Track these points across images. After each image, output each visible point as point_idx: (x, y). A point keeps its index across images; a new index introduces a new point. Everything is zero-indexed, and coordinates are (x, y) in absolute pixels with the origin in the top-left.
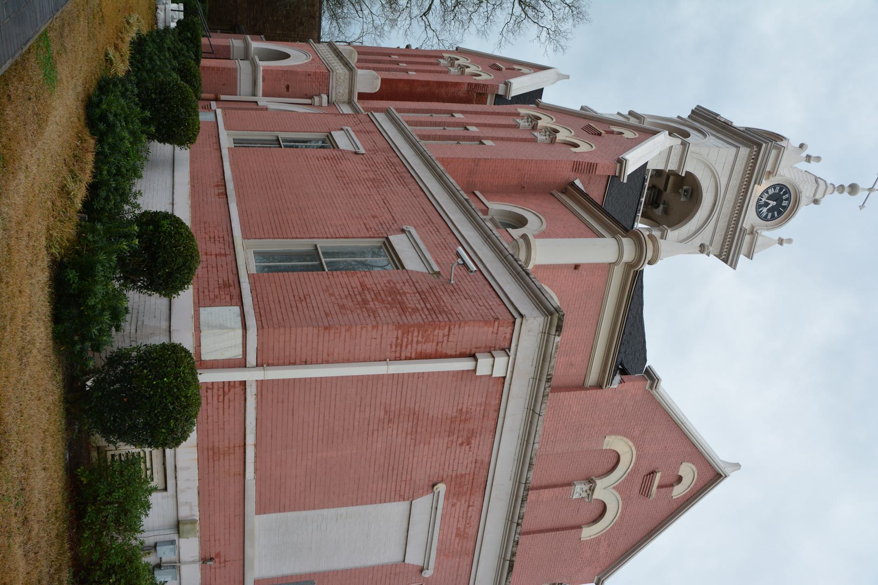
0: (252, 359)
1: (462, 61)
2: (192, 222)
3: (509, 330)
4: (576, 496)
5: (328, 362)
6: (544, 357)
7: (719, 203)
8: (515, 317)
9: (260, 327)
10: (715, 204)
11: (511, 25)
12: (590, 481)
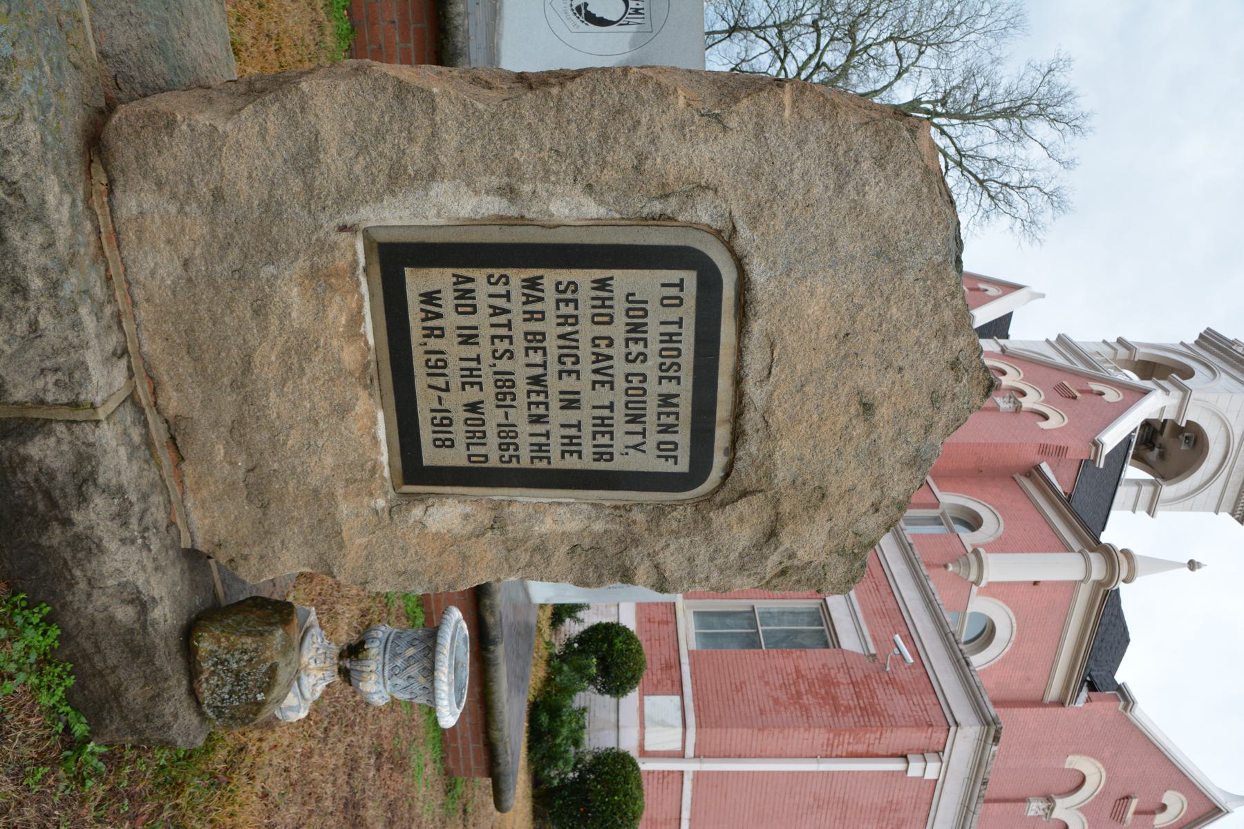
0: (690, 751)
2: (639, 622)
3: (943, 736)
4: (1031, 813)
5: (760, 757)
6: (979, 763)
7: (1229, 462)
8: (950, 724)
9: (699, 726)
10: (1225, 457)
11: (977, 218)
12: (1049, 799)
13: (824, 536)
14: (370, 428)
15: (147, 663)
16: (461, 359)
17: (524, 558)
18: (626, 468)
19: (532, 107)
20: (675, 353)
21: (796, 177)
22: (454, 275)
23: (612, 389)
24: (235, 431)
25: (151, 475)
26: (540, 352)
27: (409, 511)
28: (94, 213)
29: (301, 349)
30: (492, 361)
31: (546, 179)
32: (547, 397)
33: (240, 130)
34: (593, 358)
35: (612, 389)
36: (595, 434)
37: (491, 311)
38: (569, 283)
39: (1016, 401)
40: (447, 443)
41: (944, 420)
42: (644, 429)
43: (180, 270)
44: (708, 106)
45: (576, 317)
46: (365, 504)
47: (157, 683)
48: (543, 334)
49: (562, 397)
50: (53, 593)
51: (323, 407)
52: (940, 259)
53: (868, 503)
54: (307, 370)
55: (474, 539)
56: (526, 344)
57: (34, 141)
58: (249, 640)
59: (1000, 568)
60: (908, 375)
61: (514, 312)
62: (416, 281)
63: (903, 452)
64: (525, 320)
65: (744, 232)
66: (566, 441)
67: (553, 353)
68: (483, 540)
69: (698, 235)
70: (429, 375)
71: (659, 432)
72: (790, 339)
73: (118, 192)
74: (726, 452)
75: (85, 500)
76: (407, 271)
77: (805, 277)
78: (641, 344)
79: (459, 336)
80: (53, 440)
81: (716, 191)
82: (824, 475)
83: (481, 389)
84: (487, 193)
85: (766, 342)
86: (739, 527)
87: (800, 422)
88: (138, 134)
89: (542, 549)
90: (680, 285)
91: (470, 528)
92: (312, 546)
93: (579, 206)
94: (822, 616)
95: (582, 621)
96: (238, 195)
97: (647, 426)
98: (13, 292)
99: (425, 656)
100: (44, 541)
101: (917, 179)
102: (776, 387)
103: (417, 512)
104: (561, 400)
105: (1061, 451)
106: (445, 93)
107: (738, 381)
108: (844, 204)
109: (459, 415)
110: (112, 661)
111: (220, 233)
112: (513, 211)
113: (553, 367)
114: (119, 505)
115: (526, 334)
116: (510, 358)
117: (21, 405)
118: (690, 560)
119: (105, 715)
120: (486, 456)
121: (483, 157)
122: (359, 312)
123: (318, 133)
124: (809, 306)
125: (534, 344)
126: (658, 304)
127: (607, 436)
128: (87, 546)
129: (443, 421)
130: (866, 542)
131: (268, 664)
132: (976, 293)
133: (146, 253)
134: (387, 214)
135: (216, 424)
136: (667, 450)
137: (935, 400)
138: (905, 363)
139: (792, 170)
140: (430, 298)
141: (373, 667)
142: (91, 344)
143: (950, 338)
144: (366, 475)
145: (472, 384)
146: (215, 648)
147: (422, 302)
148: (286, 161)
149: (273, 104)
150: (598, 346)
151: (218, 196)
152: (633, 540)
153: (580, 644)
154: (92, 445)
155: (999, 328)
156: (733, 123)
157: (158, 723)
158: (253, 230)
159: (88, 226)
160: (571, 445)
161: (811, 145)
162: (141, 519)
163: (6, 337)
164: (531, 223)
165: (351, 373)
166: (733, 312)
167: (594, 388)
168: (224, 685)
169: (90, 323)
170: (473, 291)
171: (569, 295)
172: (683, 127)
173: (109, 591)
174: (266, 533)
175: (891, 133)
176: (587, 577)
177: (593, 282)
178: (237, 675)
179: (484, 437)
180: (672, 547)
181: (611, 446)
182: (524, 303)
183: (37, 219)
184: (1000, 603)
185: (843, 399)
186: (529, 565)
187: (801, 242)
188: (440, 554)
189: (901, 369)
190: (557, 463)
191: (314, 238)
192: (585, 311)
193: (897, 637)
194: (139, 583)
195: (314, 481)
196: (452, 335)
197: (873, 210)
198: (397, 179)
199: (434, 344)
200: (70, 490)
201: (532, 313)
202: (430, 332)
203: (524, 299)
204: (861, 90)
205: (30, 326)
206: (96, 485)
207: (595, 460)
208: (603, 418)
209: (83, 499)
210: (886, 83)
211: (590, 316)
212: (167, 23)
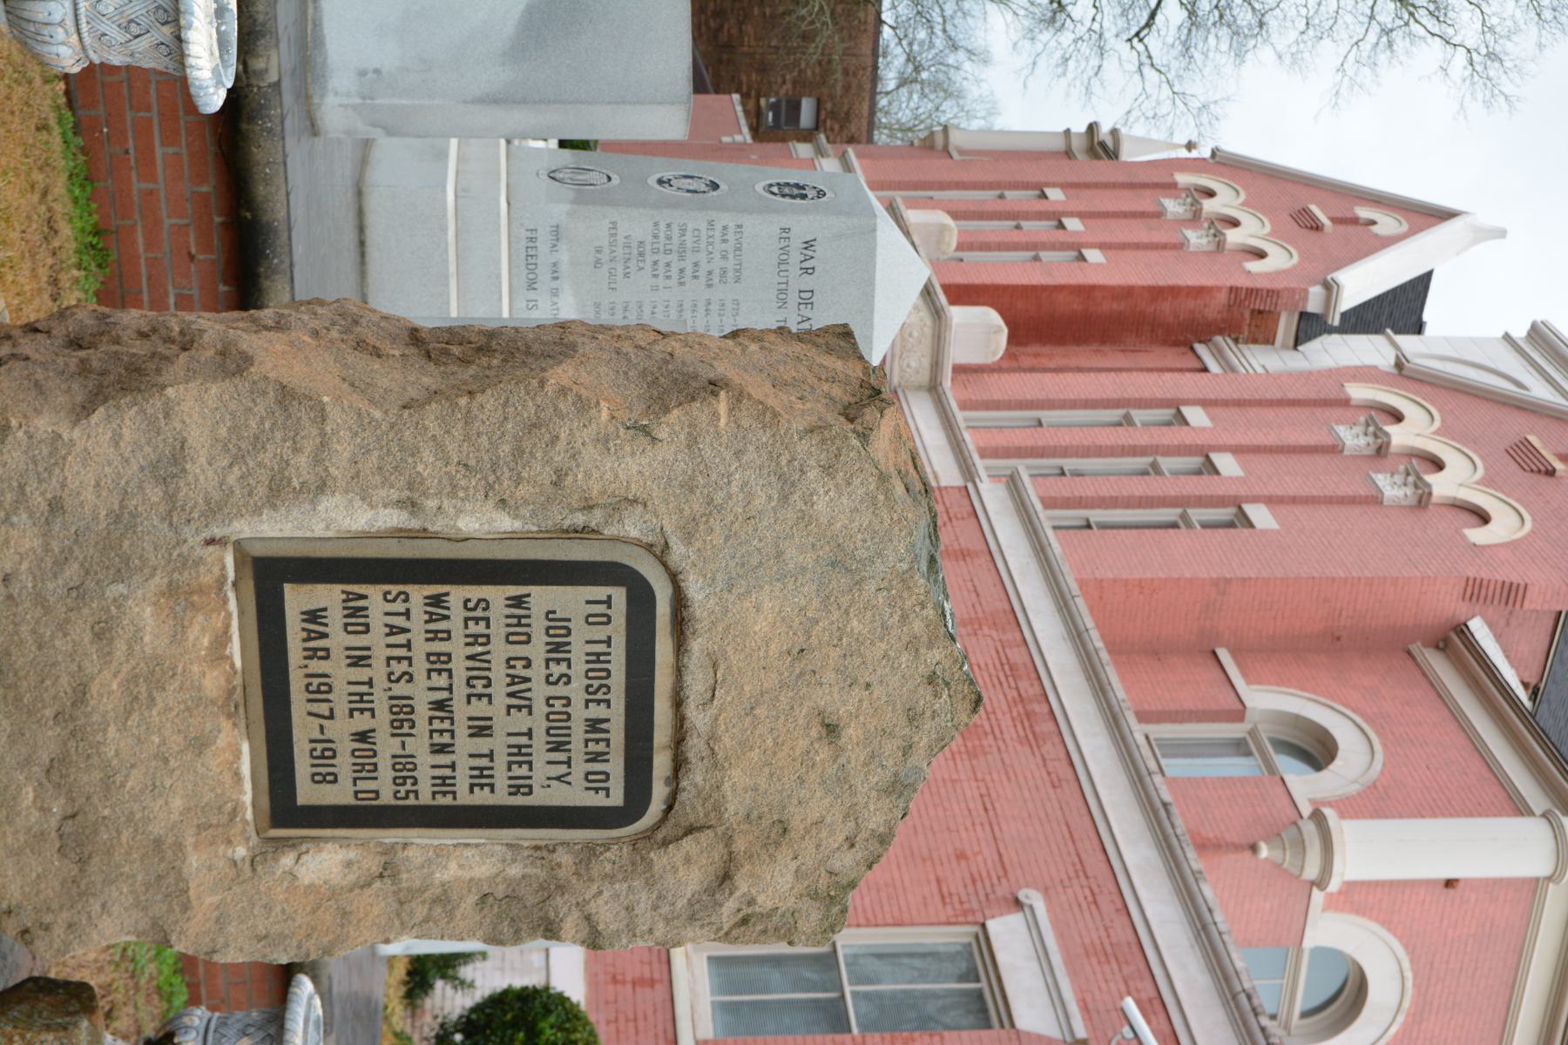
1: (1225, 201)
2: (589, 1002)
11: (1366, 47)
13: (790, 877)
17: (421, 912)
23: (530, 713)
26: (445, 675)
27: (276, 860)
29: (151, 678)
30: (387, 685)
31: (453, 493)
34: (508, 680)
35: (530, 713)
36: (510, 764)
37: (387, 630)
38: (480, 601)
39: (1419, 483)
41: (925, 740)
44: (635, 415)
45: (488, 636)
48: (449, 655)
51: (175, 742)
52: (905, 566)
53: (841, 838)
54: (159, 700)
55: (357, 891)
56: (429, 666)
59: (1368, 851)
60: (877, 691)
62: (297, 599)
63: (878, 777)
64: (428, 640)
65: (678, 550)
66: (476, 773)
68: (368, 892)
69: (628, 549)
70: (309, 701)
71: (588, 761)
72: (734, 659)
74: (667, 782)
76: (287, 587)
77: (749, 592)
78: (564, 664)
81: (645, 505)
82: (784, 808)
83: (373, 716)
84: (385, 506)
85: (707, 662)
86: (685, 869)
87: (752, 749)
89: (444, 900)
90: (608, 602)
91: (352, 877)
92: (145, 909)
94: (979, 961)
95: (471, 985)
96: (82, 504)
97: (573, 754)
101: (872, 487)
102: (721, 711)
103: (287, 860)
105: (1511, 594)
107: (678, 703)
108: (790, 515)
109: (345, 746)
112: (415, 524)
113: (460, 690)
115: (428, 655)
118: (629, 909)
120: (377, 792)
121: (380, 468)
125: (438, 666)
127: (525, 767)
129: (325, 752)
130: (845, 882)
132: (1351, 229)
134: (265, 527)
135: (27, 762)
136: (597, 782)
137: (913, 717)
138: (874, 679)
139: (729, 483)
140: (313, 616)
143: (922, 651)
144: (224, 819)
145: (362, 711)
148: (142, 469)
149: (130, 408)
151: (56, 506)
153: (467, 1035)
155: (1401, 309)
156: (663, 433)
160: (482, 778)
161: (751, 455)
164: (435, 536)
165: (213, 702)
171: (479, 613)
174: (81, 895)
175: (838, 442)
179: (375, 770)
180: (606, 894)
184: (1376, 927)
186: (426, 920)
188: (314, 911)
189: (868, 686)
190: (464, 798)
191: (175, 554)
192: (498, 630)
193: (1130, 1004)
195: (156, 829)
196: (339, 656)
198: (278, 491)
199: (316, 666)
202: (312, 654)
208: (519, 747)
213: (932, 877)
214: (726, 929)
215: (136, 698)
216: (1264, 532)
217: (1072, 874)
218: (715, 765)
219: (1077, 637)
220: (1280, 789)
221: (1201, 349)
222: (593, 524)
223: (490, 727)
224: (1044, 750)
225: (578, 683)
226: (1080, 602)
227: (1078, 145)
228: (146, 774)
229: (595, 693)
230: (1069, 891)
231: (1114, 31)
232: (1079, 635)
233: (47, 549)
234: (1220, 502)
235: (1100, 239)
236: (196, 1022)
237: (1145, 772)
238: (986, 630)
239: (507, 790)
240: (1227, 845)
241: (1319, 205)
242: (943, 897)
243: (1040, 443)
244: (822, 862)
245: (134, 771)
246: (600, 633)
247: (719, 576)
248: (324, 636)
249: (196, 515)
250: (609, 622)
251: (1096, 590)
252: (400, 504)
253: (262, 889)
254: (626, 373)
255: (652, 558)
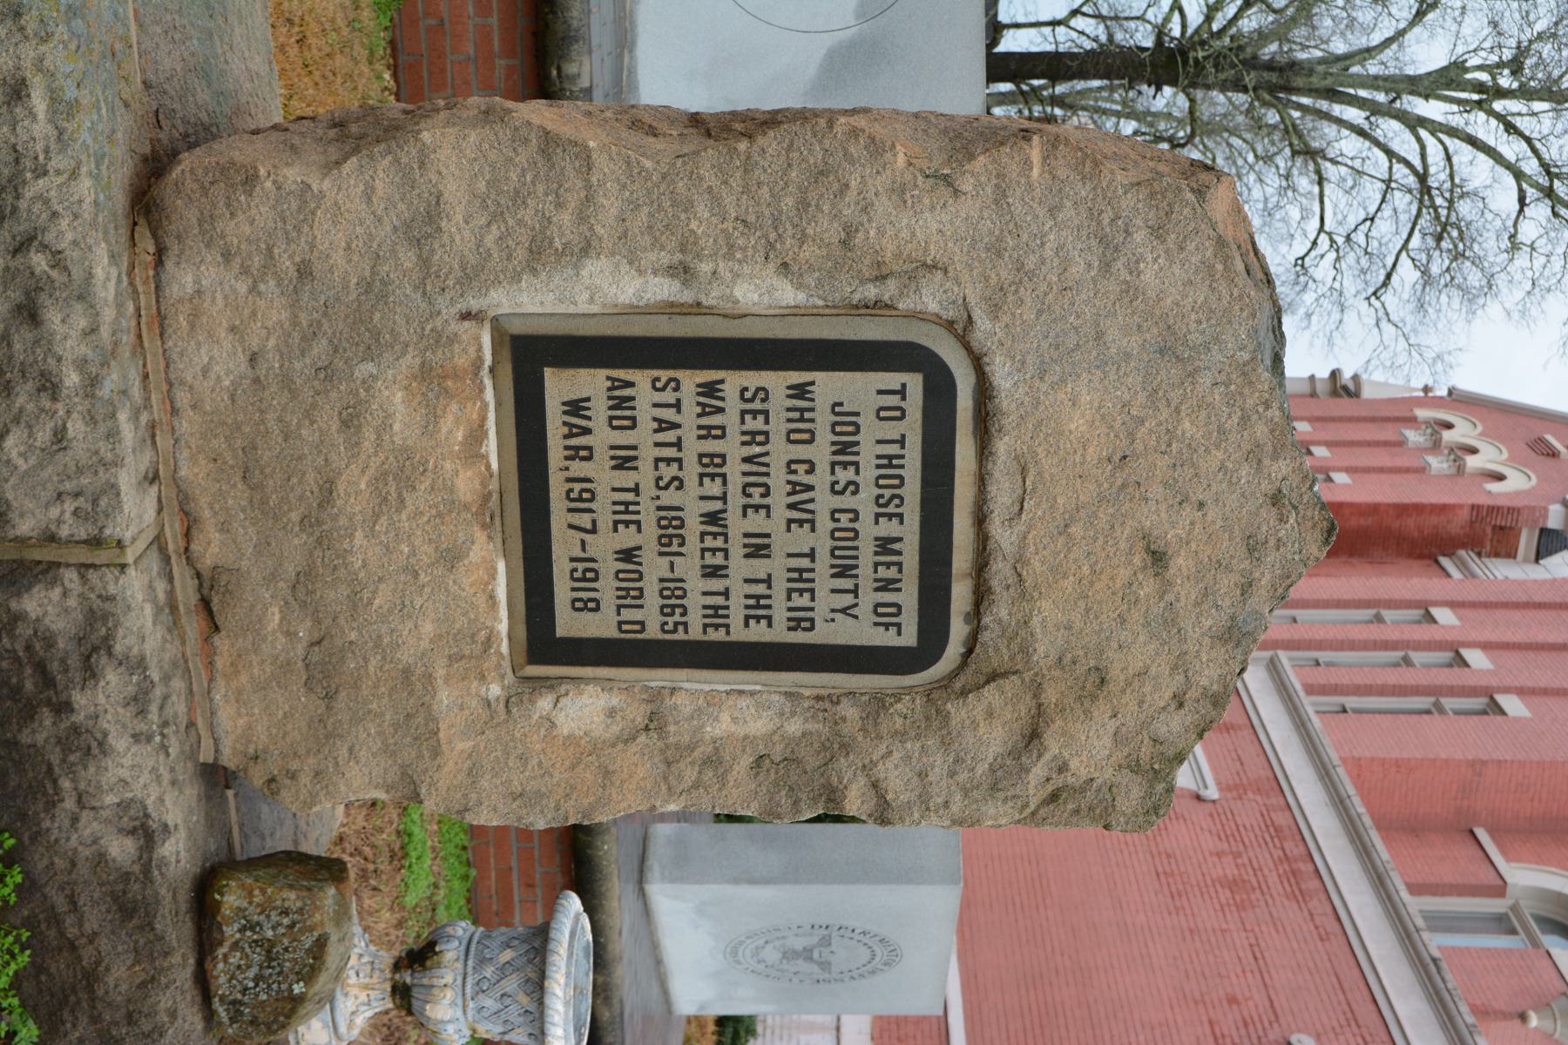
1: (1464, 430)
13: (1107, 741)
14: (487, 584)
15: (141, 928)
16: (614, 490)
17: (690, 775)
18: (832, 641)
19: (713, 166)
20: (896, 482)
21: (1048, 253)
22: (608, 378)
23: (813, 530)
24: (300, 588)
25: (173, 650)
26: (718, 480)
27: (532, 702)
28: (135, 291)
29: (402, 473)
31: (730, 256)
32: (726, 541)
33: (340, 189)
34: (789, 488)
35: (813, 530)
36: (790, 592)
37: (655, 425)
38: (758, 389)
40: (591, 605)
41: (1268, 576)
42: (856, 586)
43: (244, 367)
44: (935, 164)
45: (766, 434)
46: (473, 691)
47: (153, 960)
48: (723, 457)
49: (747, 541)
50: (23, 816)
51: (426, 552)
52: (1246, 356)
53: (1168, 694)
54: (409, 502)
55: (620, 746)
56: (701, 470)
57: (88, 200)
58: (292, 895)
60: (1212, 513)
61: (686, 427)
62: (559, 385)
64: (700, 437)
65: (982, 323)
66: (752, 602)
67: (736, 481)
68: (633, 748)
69: (925, 327)
71: (877, 590)
72: (1046, 463)
73: (169, 265)
74: (968, 618)
75: (94, 676)
76: (548, 372)
77: (1063, 381)
78: (852, 469)
79: (612, 458)
80: (58, 591)
81: (946, 271)
82: (1102, 652)
83: (639, 531)
84: (655, 273)
85: (1015, 467)
86: (987, 722)
87: (1065, 576)
88: (205, 191)
90: (902, 392)
91: (615, 729)
92: (393, 754)
93: (770, 291)
97: (860, 581)
98: (39, 390)
99: (530, 961)
100: (25, 738)
101: (1209, 254)
102: (1030, 527)
103: (545, 703)
104: (745, 546)
106: (604, 148)
107: (980, 519)
108: (1113, 287)
110: (91, 924)
111: (304, 318)
112: (687, 297)
113: (736, 500)
114: (138, 684)
115: (701, 456)
116: (679, 488)
117: (21, 541)
118: (922, 775)
119: (66, 1015)
120: (642, 623)
122: (482, 426)
123: (439, 196)
124: (1071, 419)
125: (710, 470)
126: (873, 417)
127: (807, 595)
128: (84, 744)
129: (587, 575)
131: (316, 934)
133: (199, 344)
134: (524, 298)
135: (273, 577)
136: (887, 616)
137: (1253, 547)
140: (576, 407)
141: (449, 979)
142: (127, 460)
143: (1266, 462)
146: (245, 904)
147: (565, 413)
148: (395, 229)
150: (795, 472)
151: (304, 271)
152: (843, 746)
154: (111, 599)
156: (967, 185)
157: (146, 1026)
158: (347, 317)
159: (131, 307)
160: (758, 608)
161: (1068, 212)
162: (161, 708)
163: (22, 449)
164: (710, 312)
165: (466, 507)
166: (971, 427)
167: (789, 530)
168: (249, 967)
169: (128, 434)
170: (633, 399)
171: (757, 405)
172: (903, 192)
173: (105, 814)
174: (327, 737)
175: (1170, 195)
176: (778, 805)
177: (789, 388)
178: (269, 951)
179: (641, 597)
181: (812, 609)
182: (699, 416)
183: (80, 298)
185: (1122, 545)
186: (696, 785)
187: (1057, 336)
188: (573, 767)
189: (1201, 505)
190: (739, 633)
191: (429, 327)
192: (778, 426)
194: (149, 802)
195: (405, 656)
196: (603, 457)
197: (1151, 294)
198: (540, 255)
200: (74, 661)
201: (709, 428)
202: (574, 453)
203: (699, 409)
204: (1339, 47)
205: (55, 434)
206: (110, 654)
207: (790, 629)
209: (90, 673)
210: (1389, 33)
211: (784, 432)
212: (211, 35)
213: (1205, 1019)
214: (1032, 807)
215: (385, 499)
216: (1517, 720)
217: (1344, 1022)
218: (1023, 594)
219: (1339, 803)
220: (1546, 962)
221: (1444, 561)
222: (886, 297)
223: (768, 546)
224: (1311, 905)
225: (868, 493)
226: (1341, 771)
227: (1321, 388)
228: (395, 590)
229: (886, 505)
230: (1341, 1038)
231: (1353, 291)
232: (1342, 802)
233: (295, 322)
234: (1472, 692)
235: (1346, 464)
236: (460, 932)
237: (1412, 929)
238: (1250, 795)
239: (785, 624)
240: (1495, 1012)
241: (1554, 435)
242: (1216, 1038)
243: (1296, 637)
244: (1145, 725)
245: (382, 586)
246: (892, 430)
247: (1030, 359)
248: (587, 431)
249: (450, 283)
250: (903, 417)
251: (1358, 768)
252: (672, 271)
253: (518, 735)
254: (925, 131)
255: (952, 340)
